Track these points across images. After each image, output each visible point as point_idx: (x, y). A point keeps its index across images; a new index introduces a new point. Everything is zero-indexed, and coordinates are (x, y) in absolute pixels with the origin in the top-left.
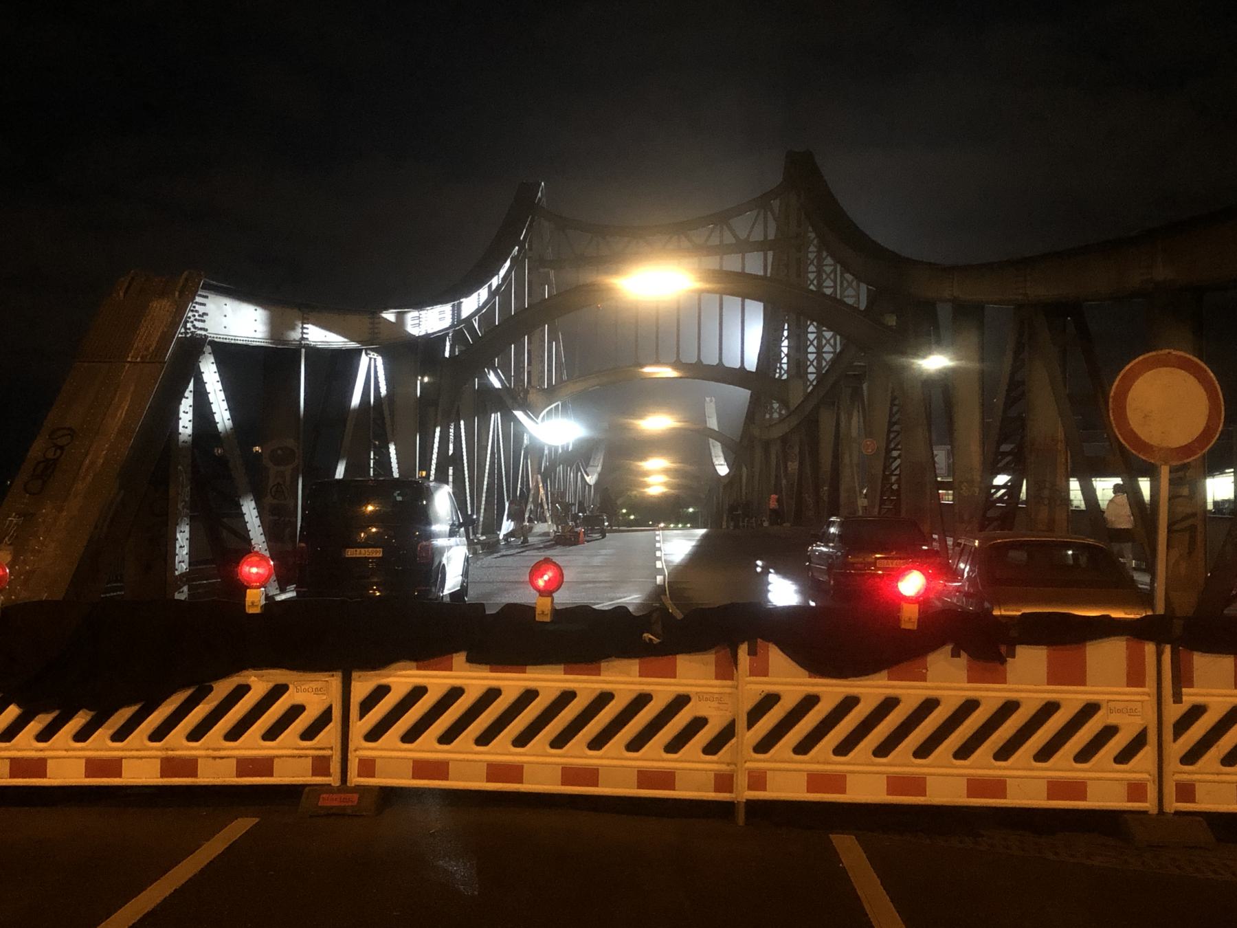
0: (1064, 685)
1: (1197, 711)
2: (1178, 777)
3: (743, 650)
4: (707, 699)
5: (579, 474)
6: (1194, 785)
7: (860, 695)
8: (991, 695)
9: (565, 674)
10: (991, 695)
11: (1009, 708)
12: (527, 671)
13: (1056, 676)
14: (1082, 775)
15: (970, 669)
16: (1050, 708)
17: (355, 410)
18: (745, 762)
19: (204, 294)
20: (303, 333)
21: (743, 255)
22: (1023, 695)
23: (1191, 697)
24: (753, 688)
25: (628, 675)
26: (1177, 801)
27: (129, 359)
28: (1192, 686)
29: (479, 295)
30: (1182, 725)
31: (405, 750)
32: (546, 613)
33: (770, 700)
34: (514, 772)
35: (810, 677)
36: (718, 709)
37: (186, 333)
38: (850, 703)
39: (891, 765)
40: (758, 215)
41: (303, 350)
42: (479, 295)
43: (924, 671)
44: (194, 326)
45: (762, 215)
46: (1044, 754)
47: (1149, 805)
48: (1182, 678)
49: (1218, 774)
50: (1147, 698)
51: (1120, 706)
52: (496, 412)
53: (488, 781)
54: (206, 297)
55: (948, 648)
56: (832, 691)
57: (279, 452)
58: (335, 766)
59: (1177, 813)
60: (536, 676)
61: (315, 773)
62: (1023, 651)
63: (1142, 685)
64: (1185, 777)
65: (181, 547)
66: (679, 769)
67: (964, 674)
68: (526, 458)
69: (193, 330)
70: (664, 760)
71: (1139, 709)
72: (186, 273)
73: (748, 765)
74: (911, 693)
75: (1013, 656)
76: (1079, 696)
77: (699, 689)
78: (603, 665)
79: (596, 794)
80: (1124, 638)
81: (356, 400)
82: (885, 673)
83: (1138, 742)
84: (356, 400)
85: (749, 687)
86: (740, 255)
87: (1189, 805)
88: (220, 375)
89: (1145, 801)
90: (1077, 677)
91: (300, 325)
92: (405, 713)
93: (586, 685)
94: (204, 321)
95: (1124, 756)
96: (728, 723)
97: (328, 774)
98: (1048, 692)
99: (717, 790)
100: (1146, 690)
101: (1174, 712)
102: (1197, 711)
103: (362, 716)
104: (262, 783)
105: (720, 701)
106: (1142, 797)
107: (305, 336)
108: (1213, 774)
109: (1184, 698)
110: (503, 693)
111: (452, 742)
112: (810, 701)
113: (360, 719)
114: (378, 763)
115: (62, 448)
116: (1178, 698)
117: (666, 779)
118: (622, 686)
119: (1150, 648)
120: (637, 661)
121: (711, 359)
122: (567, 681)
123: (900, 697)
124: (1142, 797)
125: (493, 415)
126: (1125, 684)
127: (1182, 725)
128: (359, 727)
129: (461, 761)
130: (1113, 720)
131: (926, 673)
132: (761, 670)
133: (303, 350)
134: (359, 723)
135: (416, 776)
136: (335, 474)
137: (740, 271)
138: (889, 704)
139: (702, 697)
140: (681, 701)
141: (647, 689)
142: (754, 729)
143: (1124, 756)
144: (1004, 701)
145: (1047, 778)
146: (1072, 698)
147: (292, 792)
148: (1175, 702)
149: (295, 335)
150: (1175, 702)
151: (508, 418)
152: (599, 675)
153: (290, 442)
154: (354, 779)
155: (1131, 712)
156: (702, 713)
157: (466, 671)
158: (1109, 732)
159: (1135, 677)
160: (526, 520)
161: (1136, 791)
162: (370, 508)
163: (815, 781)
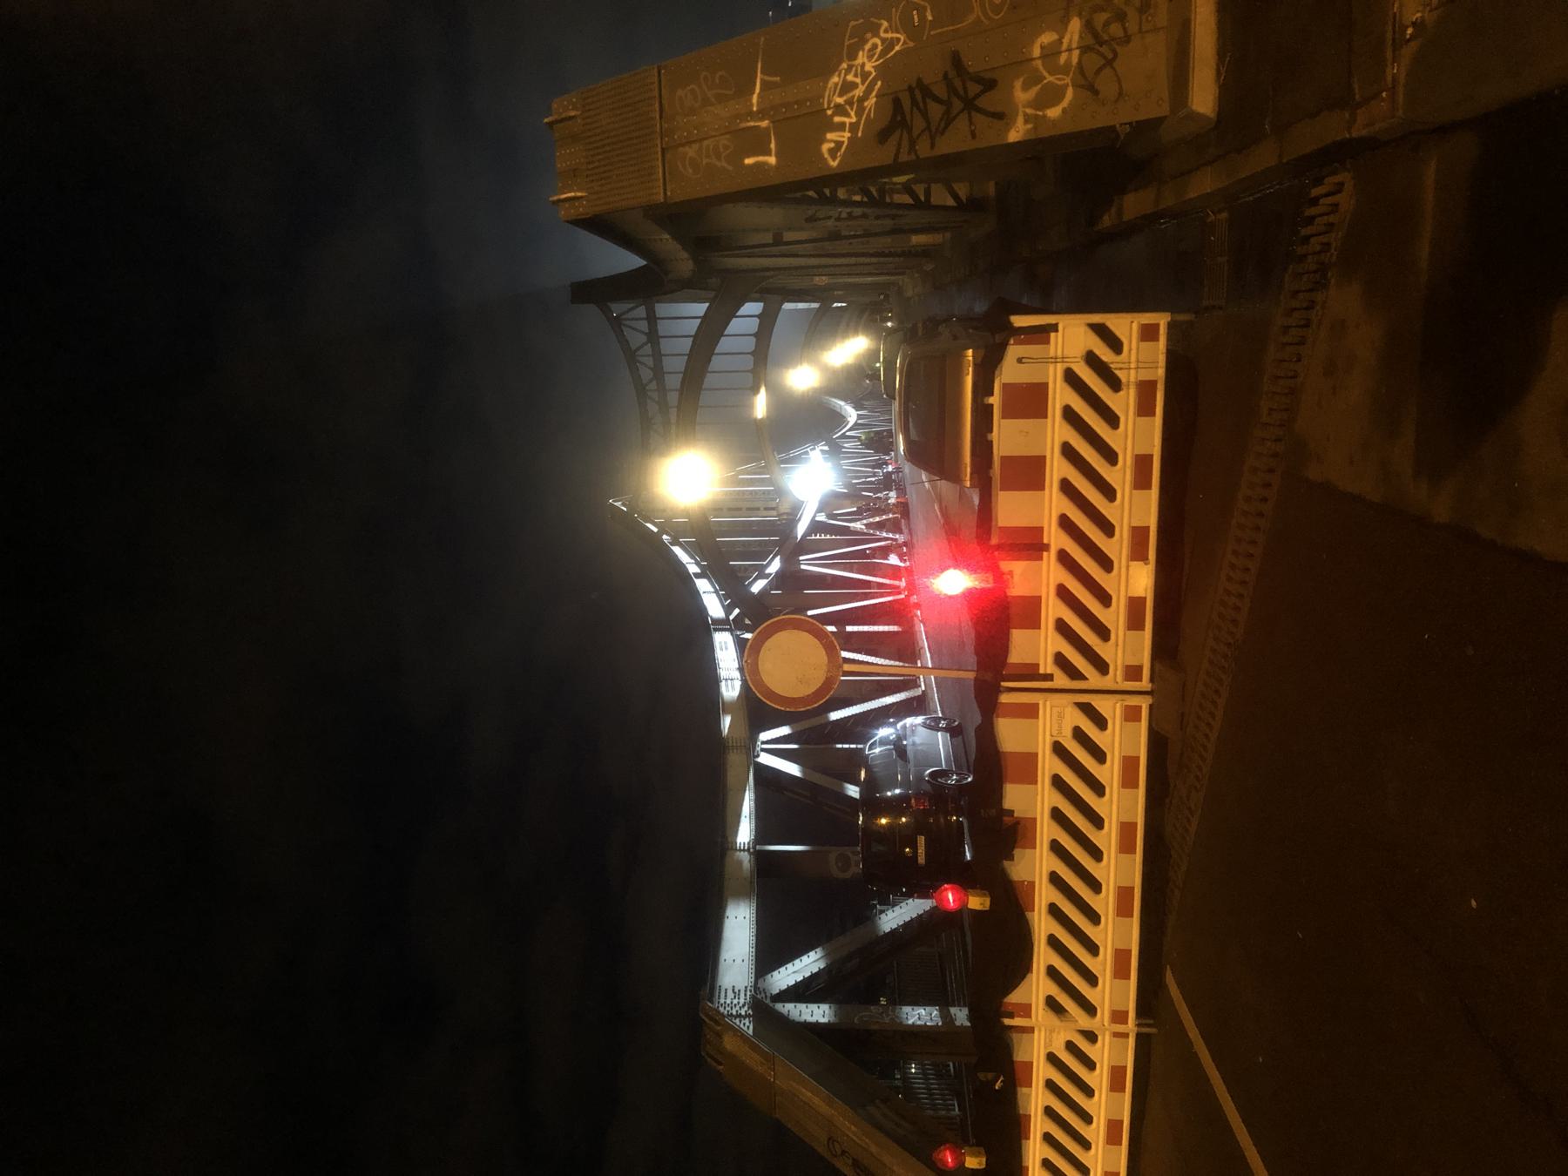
0: (1036, 827)
1: (1061, 660)
2: (1119, 679)
3: (1007, 1022)
4: (1051, 1041)
5: (848, 434)
6: (1137, 455)
7: (1051, 808)
8: (1047, 831)
9: (1034, 911)
10: (1047, 831)
11: (1057, 815)
12: (1026, 1059)
13: (1033, 621)
14: (1105, 1068)
15: (1024, 847)
16: (1058, 782)
17: (803, 772)
18: (1104, 1025)
19: (718, 991)
20: (744, 850)
21: (659, 318)
22: (1051, 580)
23: (1047, 666)
24: (1040, 1013)
25: (1030, 1095)
26: (1141, 680)
27: (772, 1080)
28: (1038, 665)
29: (704, 592)
30: (1074, 673)
31: (1120, 568)
32: (982, 902)
33: (1052, 1003)
34: (1129, 764)
35: (1032, 972)
36: (1059, 1033)
37: (749, 1016)
38: (1053, 942)
39: (1127, 416)
40: (630, 327)
41: (758, 847)
42: (704, 592)
43: (1026, 883)
44: (744, 1006)
45: (627, 323)
46: (1109, 492)
47: (1144, 703)
48: (1030, 672)
49: (1117, 645)
50: (1048, 703)
51: (1055, 727)
52: (799, 562)
53: (1132, 916)
54: (720, 986)
55: (1006, 864)
56: (1043, 956)
57: (840, 865)
58: (1134, 701)
59: (1152, 680)
60: (1031, 1161)
61: (1138, 719)
62: (1008, 804)
63: (1037, 705)
64: (1119, 673)
65: (919, 1018)
66: (1118, 817)
67: (1028, 851)
68: (834, 517)
69: (746, 1008)
70: (1098, 1127)
71: (1058, 709)
72: (701, 1015)
73: (1106, 1024)
74: (1045, 895)
75: (1013, 811)
76: (1055, 464)
77: (1048, 733)
78: (1024, 1164)
79: (1132, 1069)
80: (995, 719)
81: (793, 769)
82: (1028, 914)
83: (1088, 710)
84: (793, 769)
85: (1040, 1019)
86: (658, 321)
87: (1133, 953)
88: (780, 967)
89: (1141, 707)
90: (1029, 761)
91: (738, 853)
92: (1084, 420)
93: (1039, 1125)
94: (739, 991)
95: (1101, 723)
96: (1080, 780)
97: (1157, 326)
98: (1037, 1088)
99: (1139, 720)
100: (1041, 703)
101: (1061, 680)
102: (1061, 660)
103: (1085, 679)
104: (1142, 851)
105: (1052, 1031)
106: (1155, 327)
107: (746, 848)
108: (1117, 650)
109: (1049, 672)
110: (1053, 869)
111: (1099, 850)
112: (1052, 972)
113: (1087, 679)
114: (1139, 451)
115: (844, 1152)
116: (1049, 677)
117: (1124, 894)
118: (1040, 1101)
119: (1005, 698)
120: (1019, 1089)
121: (751, 343)
122: (1035, 1138)
123: (1062, 442)
124: (1155, 327)
125: (803, 567)
126: (1033, 850)
127: (1074, 673)
128: (1094, 679)
129: (1121, 738)
130: (1068, 732)
131: (1028, 882)
132: (1026, 1010)
133: (758, 847)
134: (1080, 1022)
135: (1128, 977)
136: (855, 799)
137: (678, 393)
138: (1054, 911)
139: (1049, 1043)
140: (1052, 1059)
141: (1041, 1083)
142: (1087, 676)
143: (1101, 723)
144: (1061, 493)
145: (1119, 788)
146: (1049, 765)
147: (1157, 744)
148: (1052, 680)
149: (746, 859)
150: (1052, 680)
151: (805, 546)
152: (1030, 1116)
153: (832, 857)
154: (1145, 684)
155: (1061, 716)
156: (1062, 1045)
157: (1031, 985)
158: (1079, 735)
159: (1031, 712)
160: (896, 583)
161: (1132, 715)
162: (884, 821)
163: (1142, 482)
